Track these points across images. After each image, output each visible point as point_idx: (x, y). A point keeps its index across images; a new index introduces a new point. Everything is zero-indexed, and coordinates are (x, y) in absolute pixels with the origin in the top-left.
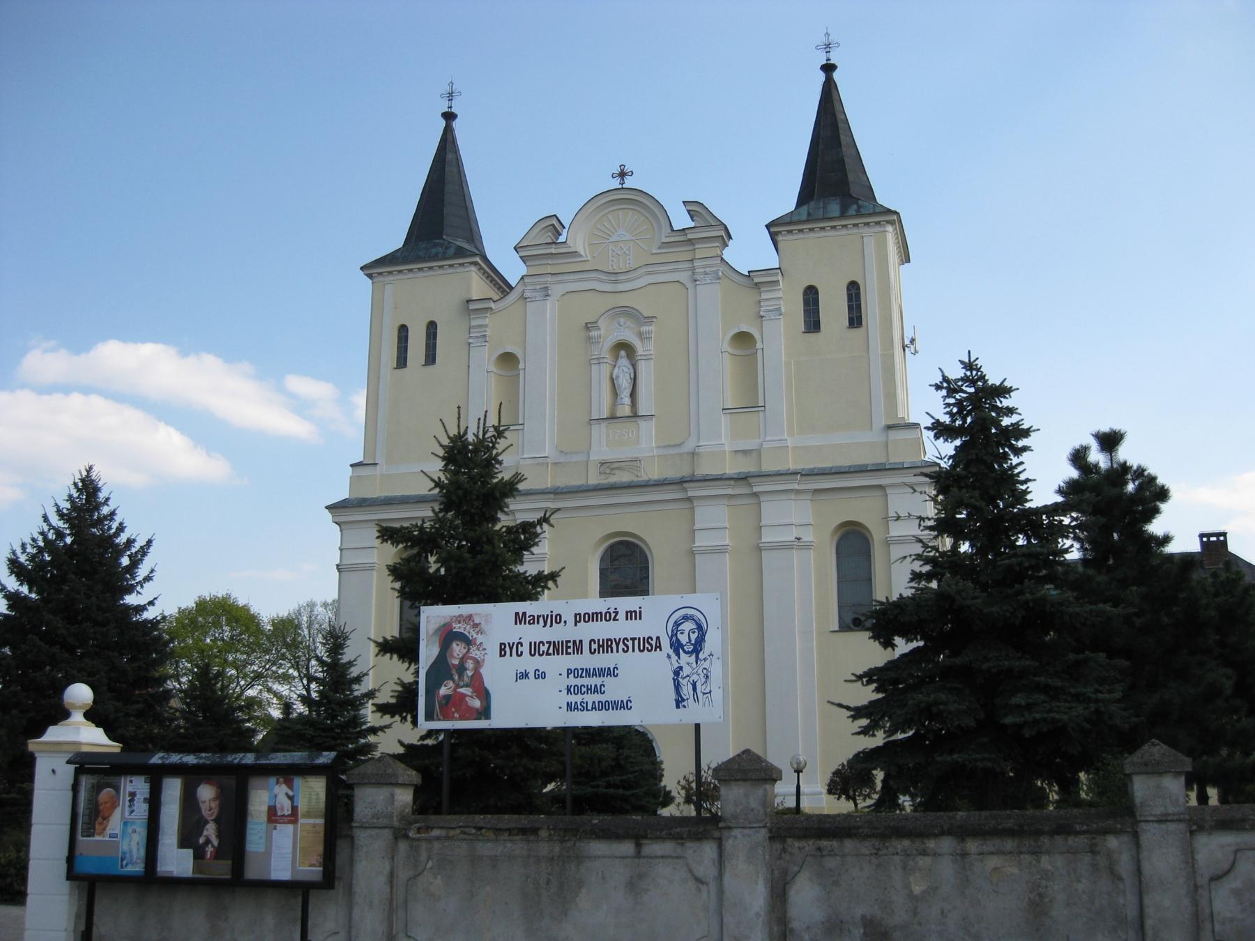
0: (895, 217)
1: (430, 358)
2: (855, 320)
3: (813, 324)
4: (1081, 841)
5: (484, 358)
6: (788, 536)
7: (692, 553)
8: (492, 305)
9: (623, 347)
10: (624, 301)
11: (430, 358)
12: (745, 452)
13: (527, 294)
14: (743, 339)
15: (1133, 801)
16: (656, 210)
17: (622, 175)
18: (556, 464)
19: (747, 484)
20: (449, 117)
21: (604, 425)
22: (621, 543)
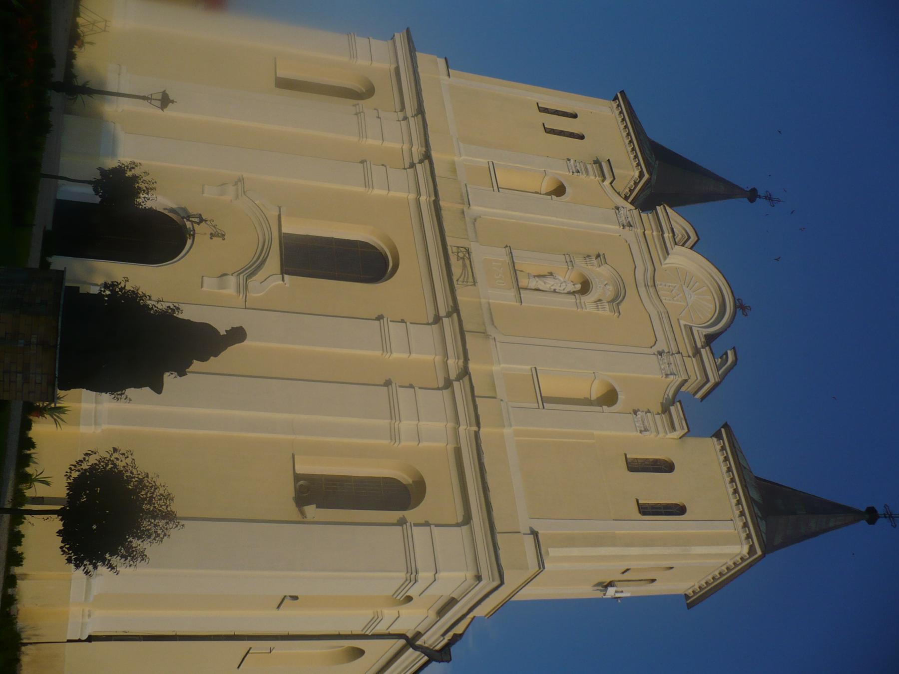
2: (647, 510)
4: (56, 99)
5: (562, 173)
7: (388, 383)
8: (607, 183)
9: (585, 287)
10: (631, 291)
12: (493, 385)
13: (622, 211)
18: (463, 212)
19: (459, 378)
20: (753, 195)
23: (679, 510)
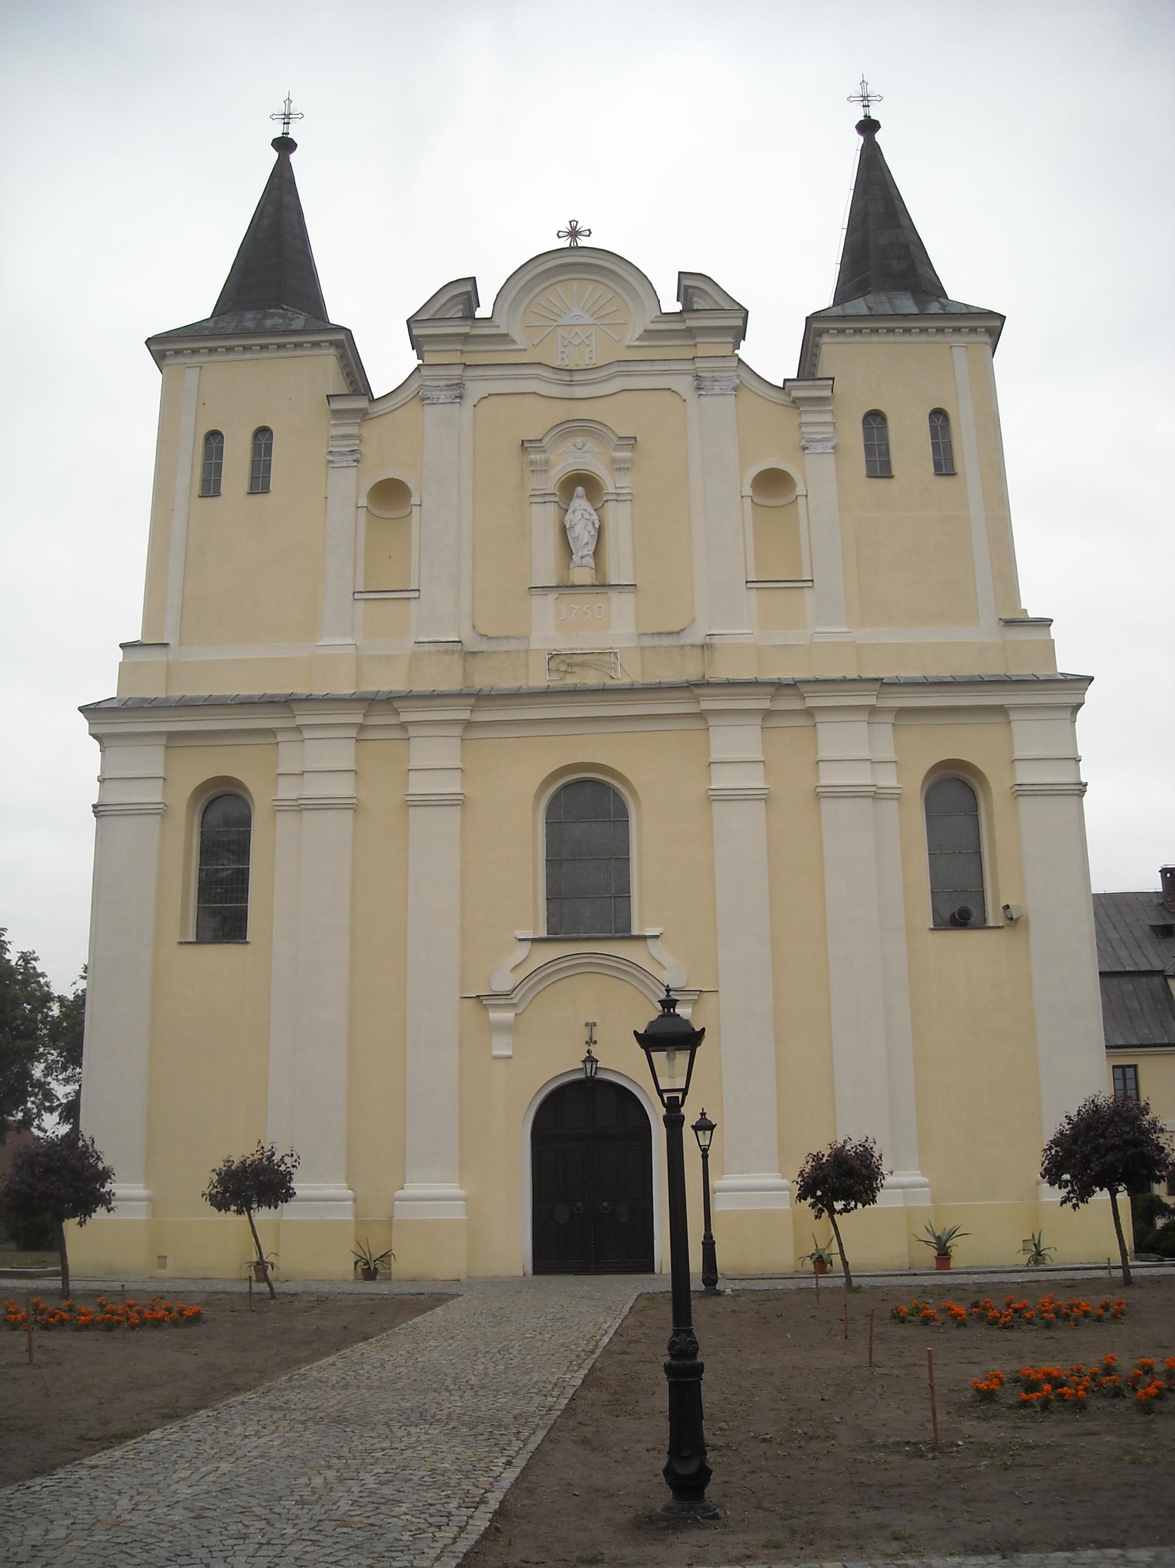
0: (341, 337)
1: (260, 482)
2: (944, 464)
3: (879, 464)
5: (348, 489)
6: (860, 777)
9: (581, 482)
10: (582, 411)
11: (260, 482)
14: (773, 482)
15: (825, 1559)
16: (635, 283)
17: (574, 233)
19: (787, 700)
20: (284, 145)
21: (552, 596)
22: (566, 787)
23: (939, 417)
